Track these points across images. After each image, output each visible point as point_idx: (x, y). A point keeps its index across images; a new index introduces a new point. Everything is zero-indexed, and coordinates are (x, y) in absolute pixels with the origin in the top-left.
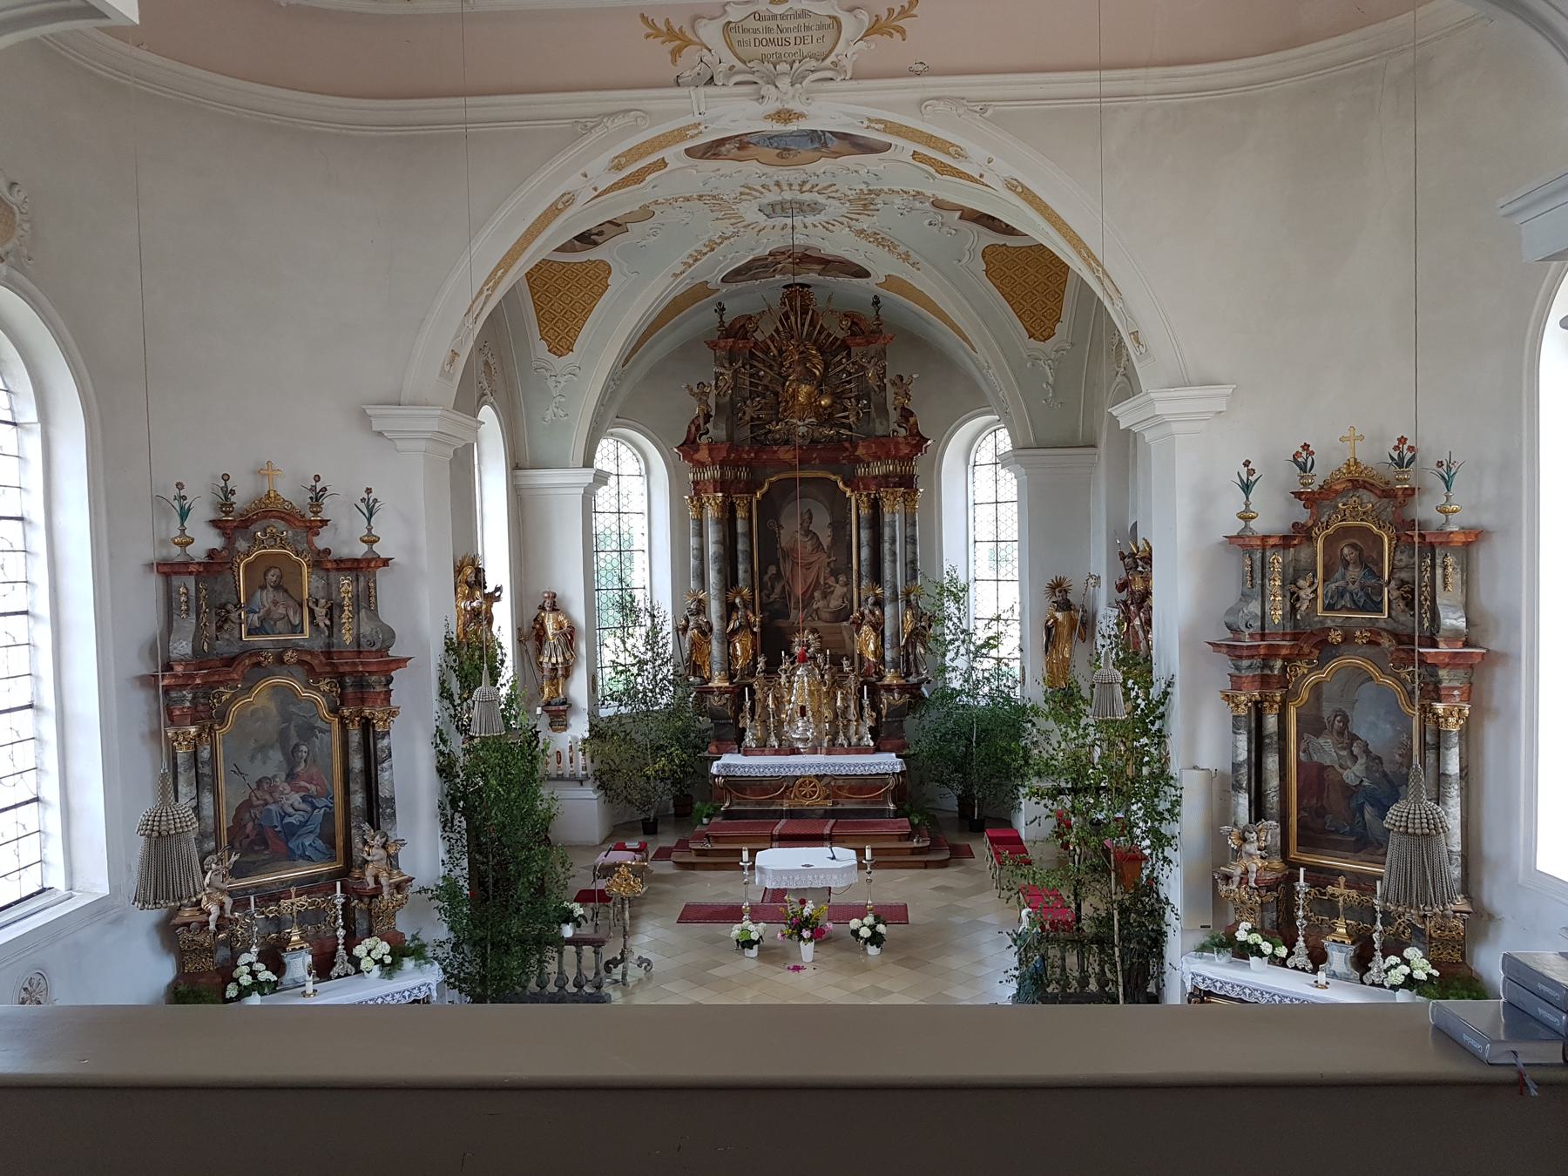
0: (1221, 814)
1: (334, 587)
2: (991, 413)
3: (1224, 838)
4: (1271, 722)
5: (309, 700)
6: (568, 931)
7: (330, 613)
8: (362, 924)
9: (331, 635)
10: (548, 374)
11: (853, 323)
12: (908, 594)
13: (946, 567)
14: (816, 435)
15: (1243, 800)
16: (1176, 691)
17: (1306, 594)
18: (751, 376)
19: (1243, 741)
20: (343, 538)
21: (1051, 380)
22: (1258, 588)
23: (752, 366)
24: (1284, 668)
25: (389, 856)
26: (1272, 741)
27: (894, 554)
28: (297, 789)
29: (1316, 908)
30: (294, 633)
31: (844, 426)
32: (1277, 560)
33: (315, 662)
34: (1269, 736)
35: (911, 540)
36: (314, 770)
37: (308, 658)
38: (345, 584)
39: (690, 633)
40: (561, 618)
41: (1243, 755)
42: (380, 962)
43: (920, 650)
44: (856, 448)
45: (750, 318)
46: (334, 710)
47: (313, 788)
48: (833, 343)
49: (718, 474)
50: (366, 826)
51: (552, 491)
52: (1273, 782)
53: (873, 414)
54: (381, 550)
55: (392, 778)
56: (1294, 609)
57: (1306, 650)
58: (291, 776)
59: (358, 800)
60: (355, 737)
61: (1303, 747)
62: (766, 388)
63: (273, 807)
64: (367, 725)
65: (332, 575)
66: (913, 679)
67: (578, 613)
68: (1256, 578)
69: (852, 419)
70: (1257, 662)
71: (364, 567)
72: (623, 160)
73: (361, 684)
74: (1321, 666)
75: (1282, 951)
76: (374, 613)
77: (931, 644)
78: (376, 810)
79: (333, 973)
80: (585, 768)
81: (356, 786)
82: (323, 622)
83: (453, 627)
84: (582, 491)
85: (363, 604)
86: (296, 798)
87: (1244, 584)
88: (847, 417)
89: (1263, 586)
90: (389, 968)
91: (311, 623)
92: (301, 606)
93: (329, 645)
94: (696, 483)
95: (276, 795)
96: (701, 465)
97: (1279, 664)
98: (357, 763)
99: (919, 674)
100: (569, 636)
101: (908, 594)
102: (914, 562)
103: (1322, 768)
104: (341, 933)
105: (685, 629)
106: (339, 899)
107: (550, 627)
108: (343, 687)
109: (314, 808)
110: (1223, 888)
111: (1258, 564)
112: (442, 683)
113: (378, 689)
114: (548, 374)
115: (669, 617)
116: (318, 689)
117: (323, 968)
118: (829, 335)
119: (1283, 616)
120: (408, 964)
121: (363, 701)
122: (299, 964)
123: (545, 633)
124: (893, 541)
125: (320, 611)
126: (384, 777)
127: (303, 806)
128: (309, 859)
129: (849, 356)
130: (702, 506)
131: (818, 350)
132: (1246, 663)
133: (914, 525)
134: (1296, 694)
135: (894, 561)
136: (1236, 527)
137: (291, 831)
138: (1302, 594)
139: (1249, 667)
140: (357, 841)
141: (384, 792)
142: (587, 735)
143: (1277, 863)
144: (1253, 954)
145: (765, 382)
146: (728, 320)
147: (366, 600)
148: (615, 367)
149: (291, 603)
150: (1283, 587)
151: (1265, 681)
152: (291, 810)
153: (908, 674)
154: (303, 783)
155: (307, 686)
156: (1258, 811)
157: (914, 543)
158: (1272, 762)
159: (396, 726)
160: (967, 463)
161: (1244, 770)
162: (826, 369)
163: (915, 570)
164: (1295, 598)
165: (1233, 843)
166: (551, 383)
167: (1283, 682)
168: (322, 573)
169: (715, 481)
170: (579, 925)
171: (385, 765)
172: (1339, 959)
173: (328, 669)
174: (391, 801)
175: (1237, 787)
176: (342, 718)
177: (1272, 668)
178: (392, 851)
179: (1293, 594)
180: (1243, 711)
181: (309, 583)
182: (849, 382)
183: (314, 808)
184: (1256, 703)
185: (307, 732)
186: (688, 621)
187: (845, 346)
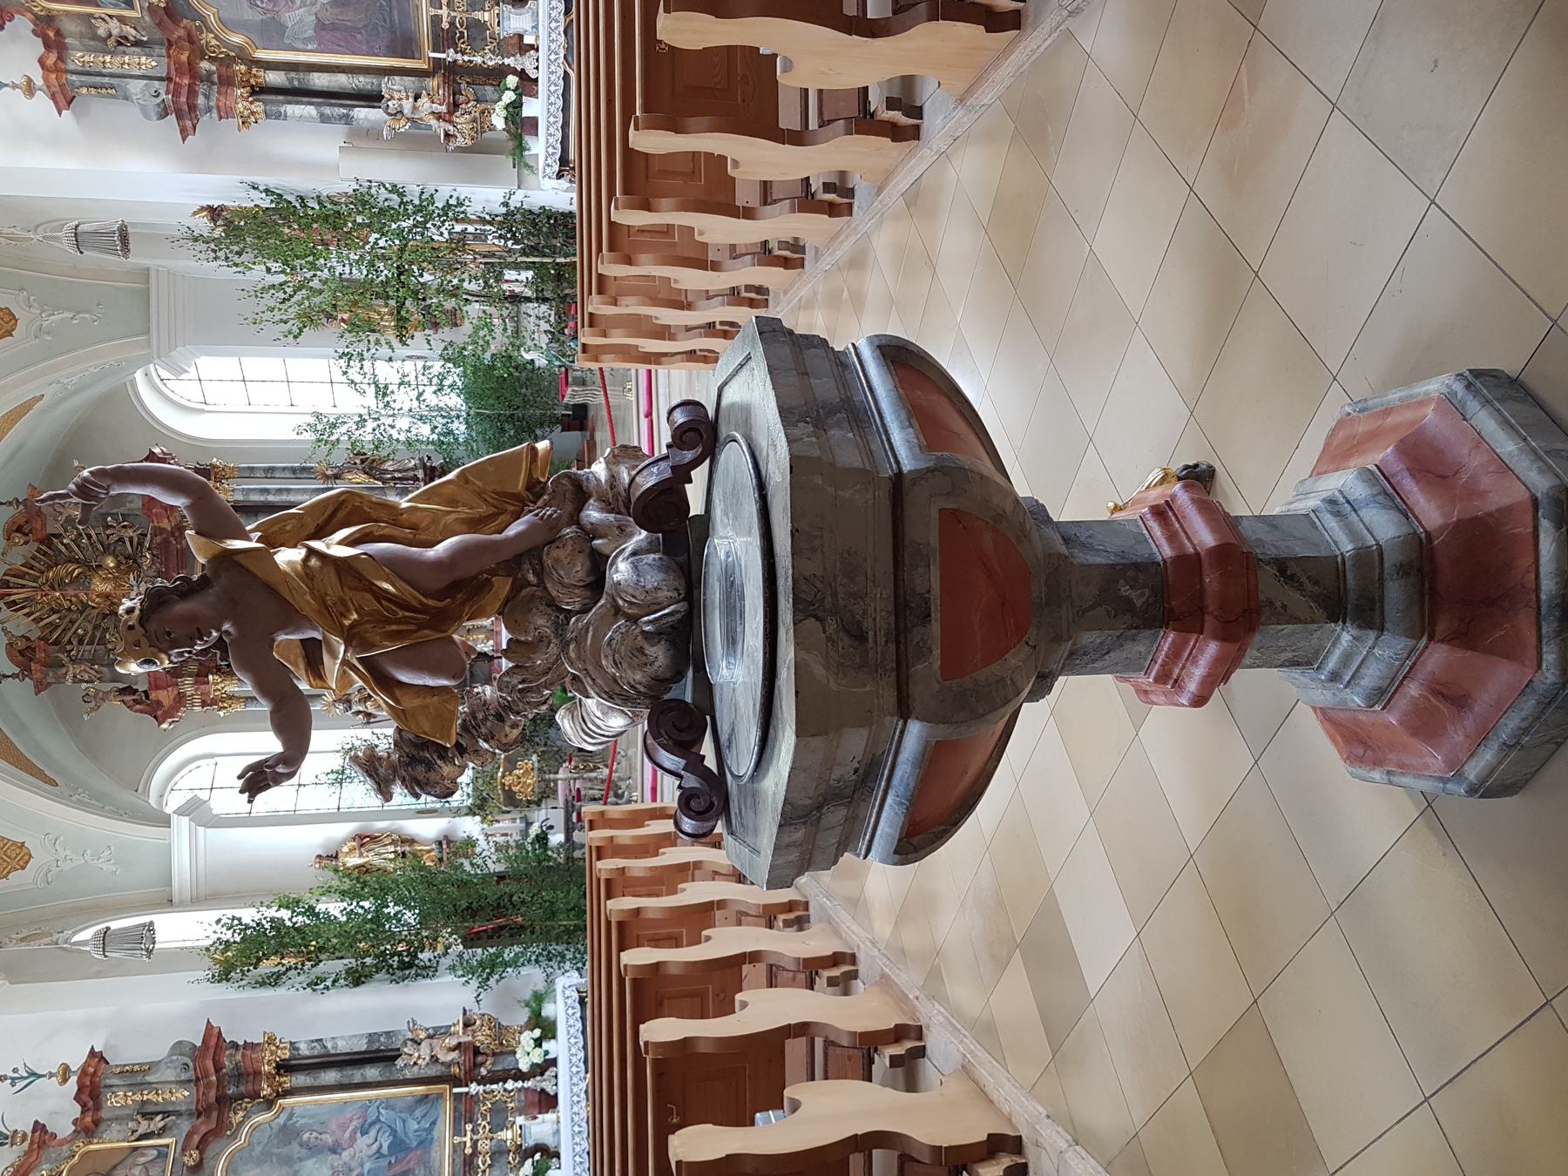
0: (366, 137)
1: (118, 1112)
2: (133, 383)
3: (397, 137)
4: (275, 78)
5: (251, 1134)
6: (557, 838)
7: (148, 1116)
8: (505, 1063)
9: (178, 1114)
10: (55, 870)
11: (19, 530)
12: (327, 477)
13: (293, 436)
14: (151, 573)
15: (362, 114)
16: (262, 180)
17: (115, 28)
18: (81, 642)
19: (294, 110)
20: (58, 1107)
21: (67, 315)
22: (112, 81)
23: (70, 642)
24: (212, 60)
25: (430, 1037)
26: (296, 80)
27: (280, 490)
28: (353, 1139)
29: (478, 43)
30: (166, 1155)
31: (140, 544)
32: (78, 58)
33: (203, 1129)
34: (291, 80)
35: (270, 472)
36: (333, 1126)
37: (196, 1138)
38: (115, 1101)
39: (371, 710)
40: (345, 849)
41: (311, 110)
42: (538, 1043)
43: (388, 466)
44: (163, 530)
45: (10, 645)
46: (269, 1103)
47: (355, 1123)
48: (45, 554)
49: (189, 680)
50: (400, 1063)
51: (201, 862)
52: (342, 81)
53: (122, 510)
54: (77, 1061)
55: (347, 1040)
56: (137, 43)
57: (182, 32)
58: (335, 1149)
59: (372, 1073)
60: (300, 1080)
61: (299, 45)
62: (96, 628)
63: (367, 1166)
64: (284, 1067)
65: (104, 1114)
66: (420, 474)
67: (344, 830)
68: (108, 85)
69: (130, 533)
70: (202, 88)
71: (92, 1083)
72: (280, 769)
73: (240, 1075)
74: (202, 18)
75: (512, 80)
76: (152, 1067)
77: (384, 453)
78: (382, 1054)
79: (550, 1090)
80: (514, 820)
81: (357, 1075)
82: (158, 1122)
83: (202, 974)
84: (201, 829)
85: (139, 1079)
86: (363, 1142)
87: (113, 96)
88: (131, 539)
89: (112, 76)
90: (548, 1030)
91: (159, 1136)
92: (136, 1149)
93: (191, 1115)
94: (204, 703)
95: (353, 1164)
96: (181, 699)
97: (205, 65)
98: (330, 1076)
99: (415, 468)
100: (364, 840)
101: (327, 477)
102: (293, 470)
103: (321, 26)
104: (510, 1085)
105: (369, 715)
106: (474, 1088)
107: (353, 861)
108: (242, 1097)
109: (378, 1120)
110: (460, 141)
111: (84, 78)
112: (262, 984)
113: (239, 1057)
114: (55, 870)
115: (353, 732)
116: (240, 1124)
117: (548, 1102)
118: (34, 558)
119: (148, 55)
120: (548, 1010)
121: (257, 1074)
122: (540, 1128)
123: (362, 866)
124: (267, 491)
125: (144, 1126)
126: (343, 1046)
127: (373, 1133)
128: (434, 1123)
129: (58, 536)
130: (231, 697)
131: (50, 568)
132: (201, 100)
133: (252, 469)
134: (241, 48)
135: (288, 490)
136: (43, 101)
137: (398, 1146)
138: (115, 32)
139: (207, 97)
140: (408, 1074)
141: (362, 1046)
142: (478, 818)
143: (433, 83)
144: (519, 114)
145: (90, 627)
146: (17, 670)
147: (136, 1076)
148: (58, 798)
149: (130, 1160)
150: (112, 53)
151: (227, 82)
152: (375, 1147)
153: (415, 479)
154: (347, 1134)
155: (234, 1136)
156: (372, 98)
157: (273, 469)
158: (320, 81)
159: (285, 1034)
160: (203, 411)
161: (327, 111)
162: (77, 561)
163: (304, 469)
164: (122, 41)
165: (403, 127)
166: (66, 866)
167: (225, 62)
168: (102, 1127)
169: (196, 682)
170: (551, 827)
171: (329, 1045)
172: (540, 1128)
173: (215, 1114)
174: (372, 1037)
175: (347, 120)
176: (279, 1096)
177: (210, 73)
178: (423, 1035)
179: (120, 44)
180: (258, 107)
181: (112, 1140)
182: (89, 536)
183: (378, 1120)
184: (253, 93)
185: (288, 1133)
186: (359, 712)
187: (47, 540)
